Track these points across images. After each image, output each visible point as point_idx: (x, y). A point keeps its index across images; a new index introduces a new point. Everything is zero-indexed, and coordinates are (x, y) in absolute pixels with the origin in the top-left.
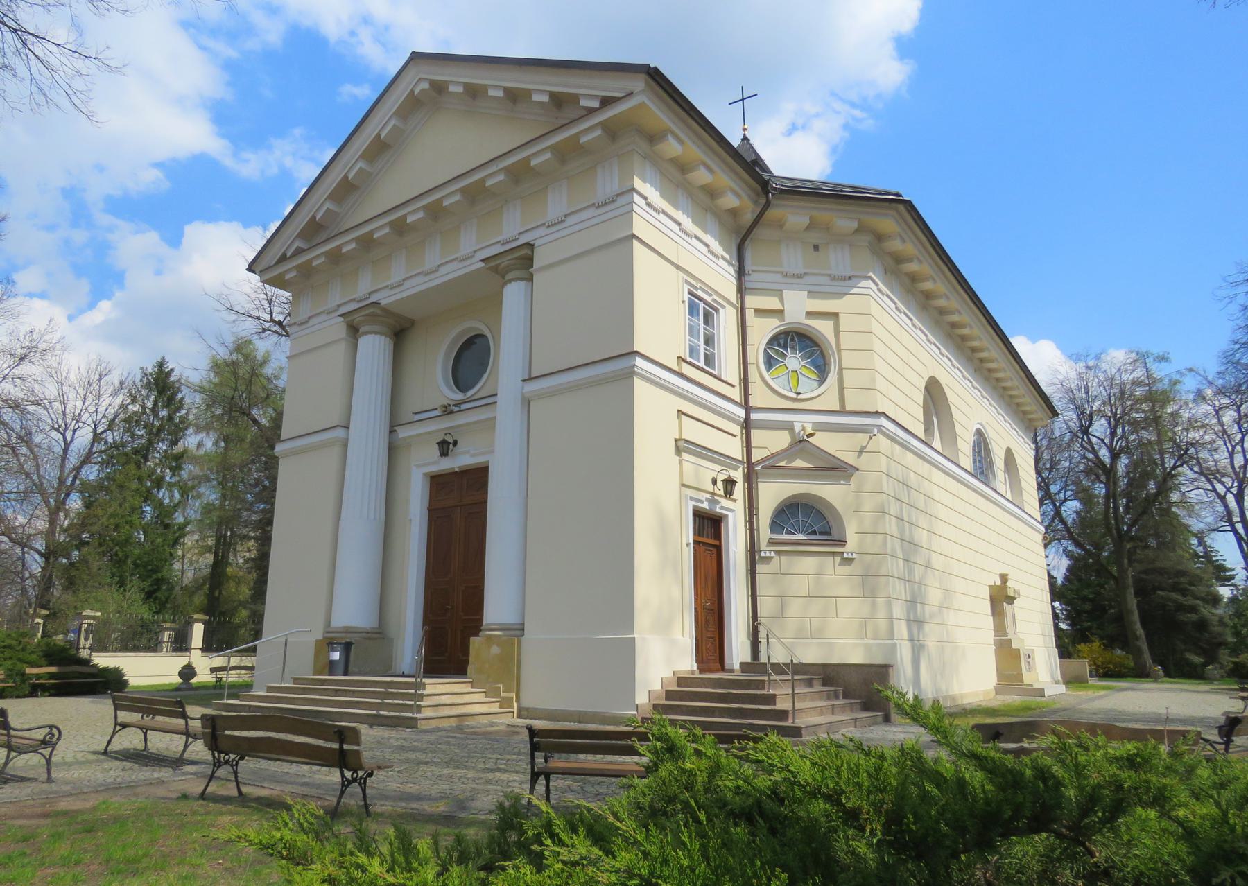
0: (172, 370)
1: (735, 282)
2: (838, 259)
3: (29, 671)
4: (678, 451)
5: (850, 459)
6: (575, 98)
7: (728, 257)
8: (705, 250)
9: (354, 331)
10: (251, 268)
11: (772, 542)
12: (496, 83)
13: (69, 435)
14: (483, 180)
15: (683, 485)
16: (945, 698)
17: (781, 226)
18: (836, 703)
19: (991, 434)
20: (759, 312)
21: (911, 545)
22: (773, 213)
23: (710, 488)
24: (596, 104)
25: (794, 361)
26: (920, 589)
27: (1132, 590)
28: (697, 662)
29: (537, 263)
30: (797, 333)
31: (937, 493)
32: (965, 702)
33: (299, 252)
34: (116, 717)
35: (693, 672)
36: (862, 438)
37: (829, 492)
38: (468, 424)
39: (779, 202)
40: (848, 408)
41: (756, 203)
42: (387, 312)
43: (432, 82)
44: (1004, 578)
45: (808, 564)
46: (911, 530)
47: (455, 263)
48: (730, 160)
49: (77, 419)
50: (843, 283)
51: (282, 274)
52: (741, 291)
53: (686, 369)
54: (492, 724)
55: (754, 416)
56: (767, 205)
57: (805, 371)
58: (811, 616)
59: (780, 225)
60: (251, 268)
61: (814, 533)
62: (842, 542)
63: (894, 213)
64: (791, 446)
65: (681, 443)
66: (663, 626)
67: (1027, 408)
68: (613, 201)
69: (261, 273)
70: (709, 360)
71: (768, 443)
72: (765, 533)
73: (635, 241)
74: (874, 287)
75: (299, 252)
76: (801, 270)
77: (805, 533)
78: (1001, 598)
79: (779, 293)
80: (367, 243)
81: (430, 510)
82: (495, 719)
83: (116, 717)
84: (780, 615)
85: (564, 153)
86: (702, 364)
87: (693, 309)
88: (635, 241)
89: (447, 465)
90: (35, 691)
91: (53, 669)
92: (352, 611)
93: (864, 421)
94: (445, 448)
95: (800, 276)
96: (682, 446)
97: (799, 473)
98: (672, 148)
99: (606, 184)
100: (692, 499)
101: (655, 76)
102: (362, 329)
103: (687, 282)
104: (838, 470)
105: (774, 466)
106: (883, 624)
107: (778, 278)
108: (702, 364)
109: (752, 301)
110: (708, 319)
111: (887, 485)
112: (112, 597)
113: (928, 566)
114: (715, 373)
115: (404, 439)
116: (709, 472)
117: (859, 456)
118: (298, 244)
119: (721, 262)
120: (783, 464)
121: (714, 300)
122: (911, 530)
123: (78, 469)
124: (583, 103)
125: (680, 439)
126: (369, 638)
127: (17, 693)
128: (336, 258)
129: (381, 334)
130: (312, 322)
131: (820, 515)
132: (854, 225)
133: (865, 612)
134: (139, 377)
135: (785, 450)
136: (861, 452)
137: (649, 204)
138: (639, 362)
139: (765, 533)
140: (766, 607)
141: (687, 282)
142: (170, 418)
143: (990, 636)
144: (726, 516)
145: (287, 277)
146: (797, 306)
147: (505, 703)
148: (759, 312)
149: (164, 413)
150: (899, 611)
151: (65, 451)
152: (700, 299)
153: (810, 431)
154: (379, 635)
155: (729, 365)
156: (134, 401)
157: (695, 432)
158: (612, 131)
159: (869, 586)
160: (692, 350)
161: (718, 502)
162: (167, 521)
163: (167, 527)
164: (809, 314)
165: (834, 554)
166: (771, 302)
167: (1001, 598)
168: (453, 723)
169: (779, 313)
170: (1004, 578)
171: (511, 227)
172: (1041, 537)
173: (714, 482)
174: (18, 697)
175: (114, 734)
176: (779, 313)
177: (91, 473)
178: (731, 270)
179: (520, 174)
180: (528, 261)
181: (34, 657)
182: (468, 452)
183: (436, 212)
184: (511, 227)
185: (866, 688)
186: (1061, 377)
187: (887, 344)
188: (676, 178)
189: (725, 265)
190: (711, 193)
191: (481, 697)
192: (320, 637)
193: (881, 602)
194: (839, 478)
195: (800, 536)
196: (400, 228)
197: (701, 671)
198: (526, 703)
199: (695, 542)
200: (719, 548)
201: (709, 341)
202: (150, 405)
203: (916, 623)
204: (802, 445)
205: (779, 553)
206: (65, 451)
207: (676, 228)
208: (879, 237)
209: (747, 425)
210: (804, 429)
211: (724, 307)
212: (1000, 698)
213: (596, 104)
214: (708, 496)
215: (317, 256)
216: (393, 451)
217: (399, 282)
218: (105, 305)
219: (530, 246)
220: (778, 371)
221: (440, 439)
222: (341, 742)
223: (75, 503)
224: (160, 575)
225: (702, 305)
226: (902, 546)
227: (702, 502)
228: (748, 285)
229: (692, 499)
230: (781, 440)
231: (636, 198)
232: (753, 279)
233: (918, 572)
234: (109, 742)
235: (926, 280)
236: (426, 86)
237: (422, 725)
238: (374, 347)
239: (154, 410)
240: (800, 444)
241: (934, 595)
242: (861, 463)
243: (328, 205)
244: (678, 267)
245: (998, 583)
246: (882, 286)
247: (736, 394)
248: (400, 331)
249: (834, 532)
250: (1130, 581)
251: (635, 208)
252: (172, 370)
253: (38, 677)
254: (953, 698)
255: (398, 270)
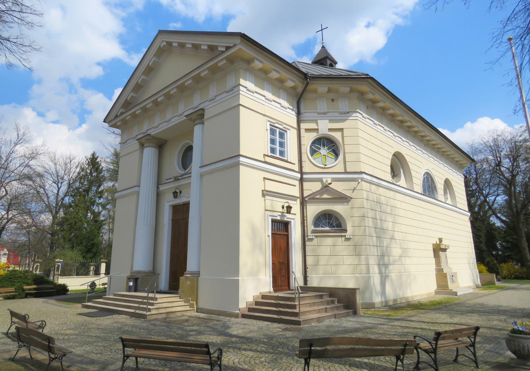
0: (98, 157)
1: (296, 118)
2: (343, 105)
3: (26, 287)
4: (264, 195)
5: (348, 193)
6: (217, 47)
7: (291, 107)
8: (279, 106)
9: (142, 146)
10: (104, 121)
11: (313, 232)
12: (189, 41)
13: (60, 185)
14: (184, 83)
15: (266, 210)
16: (402, 299)
17: (316, 92)
18: (328, 307)
19: (434, 174)
20: (307, 130)
21: (381, 232)
22: (311, 87)
23: (281, 210)
24: (224, 49)
25: (324, 151)
26: (387, 250)
27: (525, 239)
28: (273, 287)
29: (206, 117)
30: (326, 138)
31: (398, 204)
32: (415, 299)
33: (122, 113)
34: (12, 319)
35: (270, 292)
36: (353, 184)
37: (338, 208)
38: (183, 185)
39: (312, 82)
40: (348, 171)
41: (303, 83)
42: (154, 138)
43: (167, 42)
44: (441, 240)
45: (329, 241)
46: (381, 223)
47: (177, 117)
48: (287, 67)
49: (62, 178)
50: (345, 115)
51: (116, 123)
52: (299, 122)
53: (268, 160)
54: (183, 315)
55: (305, 176)
56: (308, 83)
57: (329, 155)
58: (330, 265)
59: (316, 91)
60: (104, 121)
61: (334, 227)
62: (345, 231)
63: (366, 83)
64: (322, 189)
65: (264, 192)
66: (254, 274)
67: (457, 159)
68: (233, 90)
69: (108, 123)
70: (282, 153)
71: (311, 188)
72: (310, 227)
73: (241, 107)
74: (360, 116)
75: (122, 113)
76: (326, 111)
77: (329, 227)
78: (438, 250)
79: (316, 121)
80: (145, 110)
81: (173, 220)
82: (185, 314)
83: (12, 319)
84: (316, 264)
85: (214, 70)
86: (278, 155)
87: (273, 132)
88: (241, 107)
89: (178, 201)
90: (28, 295)
91: (35, 286)
92: (141, 263)
93: (354, 176)
94: (175, 195)
95: (325, 113)
96: (265, 193)
97: (325, 201)
98: (257, 65)
99: (230, 83)
100: (270, 216)
101: (244, 37)
102: (145, 145)
103: (269, 121)
104: (343, 199)
105: (314, 198)
106: (364, 268)
107: (316, 114)
108: (278, 155)
109: (303, 126)
110: (282, 136)
111: (366, 204)
112: (70, 253)
113: (392, 238)
114: (286, 159)
115: (163, 190)
116: (278, 204)
117: (353, 192)
118: (121, 110)
119: (288, 110)
120: (318, 197)
121: (284, 127)
122: (381, 223)
123: (63, 199)
124: (220, 49)
125: (265, 190)
126: (147, 275)
127: (20, 296)
128: (134, 116)
129: (152, 147)
130: (128, 142)
131: (337, 219)
132: (349, 89)
133: (356, 262)
134: (85, 160)
135: (318, 191)
136: (354, 190)
137: (248, 90)
138: (242, 159)
139: (310, 227)
140: (310, 260)
141: (269, 121)
142: (97, 176)
143: (433, 267)
144: (291, 222)
145: (118, 124)
146: (324, 127)
147: (191, 306)
148: (307, 130)
149: (95, 174)
150: (373, 261)
151: (58, 191)
152: (277, 127)
153: (329, 182)
154: (154, 273)
155: (292, 153)
156: (83, 171)
157: (271, 186)
158: (231, 60)
159: (357, 251)
160: (273, 150)
161: (285, 216)
162: (96, 219)
163: (96, 221)
164: (330, 130)
165: (342, 236)
166: (313, 126)
167: (438, 250)
168: (164, 316)
169: (316, 130)
170: (441, 240)
171: (197, 101)
172: (468, 218)
173: (283, 207)
174: (20, 298)
175: (11, 326)
176: (316, 130)
177: (67, 200)
178: (294, 113)
179: (198, 79)
180: (202, 116)
181: (30, 281)
182: (184, 196)
183: (168, 96)
184: (197, 101)
185: (345, 300)
186: (485, 141)
187: (370, 141)
188: (262, 78)
189: (290, 111)
190: (281, 81)
191: (183, 303)
192: (129, 275)
193: (363, 257)
194: (343, 202)
195: (327, 228)
196: (156, 103)
197: (275, 291)
198: (201, 306)
199: (272, 234)
200: (287, 236)
201: (282, 145)
202: (89, 171)
203: (383, 265)
204: (326, 188)
205: (316, 236)
206: (58, 191)
207: (263, 98)
208: (362, 94)
209: (302, 180)
210: (327, 181)
211: (289, 130)
212: (437, 296)
213: (224, 49)
214: (280, 214)
215: (127, 115)
216: (158, 195)
217: (158, 125)
218: (84, 126)
219: (203, 110)
220: (316, 156)
221: (174, 191)
222: (49, 343)
223: (61, 214)
224: (93, 242)
225: (278, 130)
226: (376, 231)
227: (277, 217)
228: (302, 119)
229: (270, 216)
230: (318, 186)
231: (241, 88)
232: (304, 116)
233: (385, 243)
234: (9, 329)
235: (389, 109)
236: (165, 43)
237: (149, 318)
238: (150, 153)
239: (91, 173)
240: (326, 188)
241: (396, 251)
242: (352, 195)
243: (132, 94)
244: (264, 115)
245: (438, 243)
246: (364, 115)
247: (296, 168)
248: (161, 145)
249: (343, 225)
250: (524, 234)
251: (241, 92)
252: (98, 157)
253: (29, 290)
254: (406, 298)
255: (157, 121)
